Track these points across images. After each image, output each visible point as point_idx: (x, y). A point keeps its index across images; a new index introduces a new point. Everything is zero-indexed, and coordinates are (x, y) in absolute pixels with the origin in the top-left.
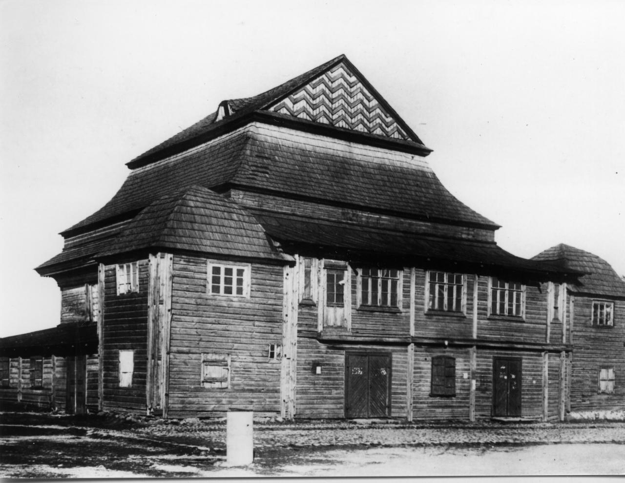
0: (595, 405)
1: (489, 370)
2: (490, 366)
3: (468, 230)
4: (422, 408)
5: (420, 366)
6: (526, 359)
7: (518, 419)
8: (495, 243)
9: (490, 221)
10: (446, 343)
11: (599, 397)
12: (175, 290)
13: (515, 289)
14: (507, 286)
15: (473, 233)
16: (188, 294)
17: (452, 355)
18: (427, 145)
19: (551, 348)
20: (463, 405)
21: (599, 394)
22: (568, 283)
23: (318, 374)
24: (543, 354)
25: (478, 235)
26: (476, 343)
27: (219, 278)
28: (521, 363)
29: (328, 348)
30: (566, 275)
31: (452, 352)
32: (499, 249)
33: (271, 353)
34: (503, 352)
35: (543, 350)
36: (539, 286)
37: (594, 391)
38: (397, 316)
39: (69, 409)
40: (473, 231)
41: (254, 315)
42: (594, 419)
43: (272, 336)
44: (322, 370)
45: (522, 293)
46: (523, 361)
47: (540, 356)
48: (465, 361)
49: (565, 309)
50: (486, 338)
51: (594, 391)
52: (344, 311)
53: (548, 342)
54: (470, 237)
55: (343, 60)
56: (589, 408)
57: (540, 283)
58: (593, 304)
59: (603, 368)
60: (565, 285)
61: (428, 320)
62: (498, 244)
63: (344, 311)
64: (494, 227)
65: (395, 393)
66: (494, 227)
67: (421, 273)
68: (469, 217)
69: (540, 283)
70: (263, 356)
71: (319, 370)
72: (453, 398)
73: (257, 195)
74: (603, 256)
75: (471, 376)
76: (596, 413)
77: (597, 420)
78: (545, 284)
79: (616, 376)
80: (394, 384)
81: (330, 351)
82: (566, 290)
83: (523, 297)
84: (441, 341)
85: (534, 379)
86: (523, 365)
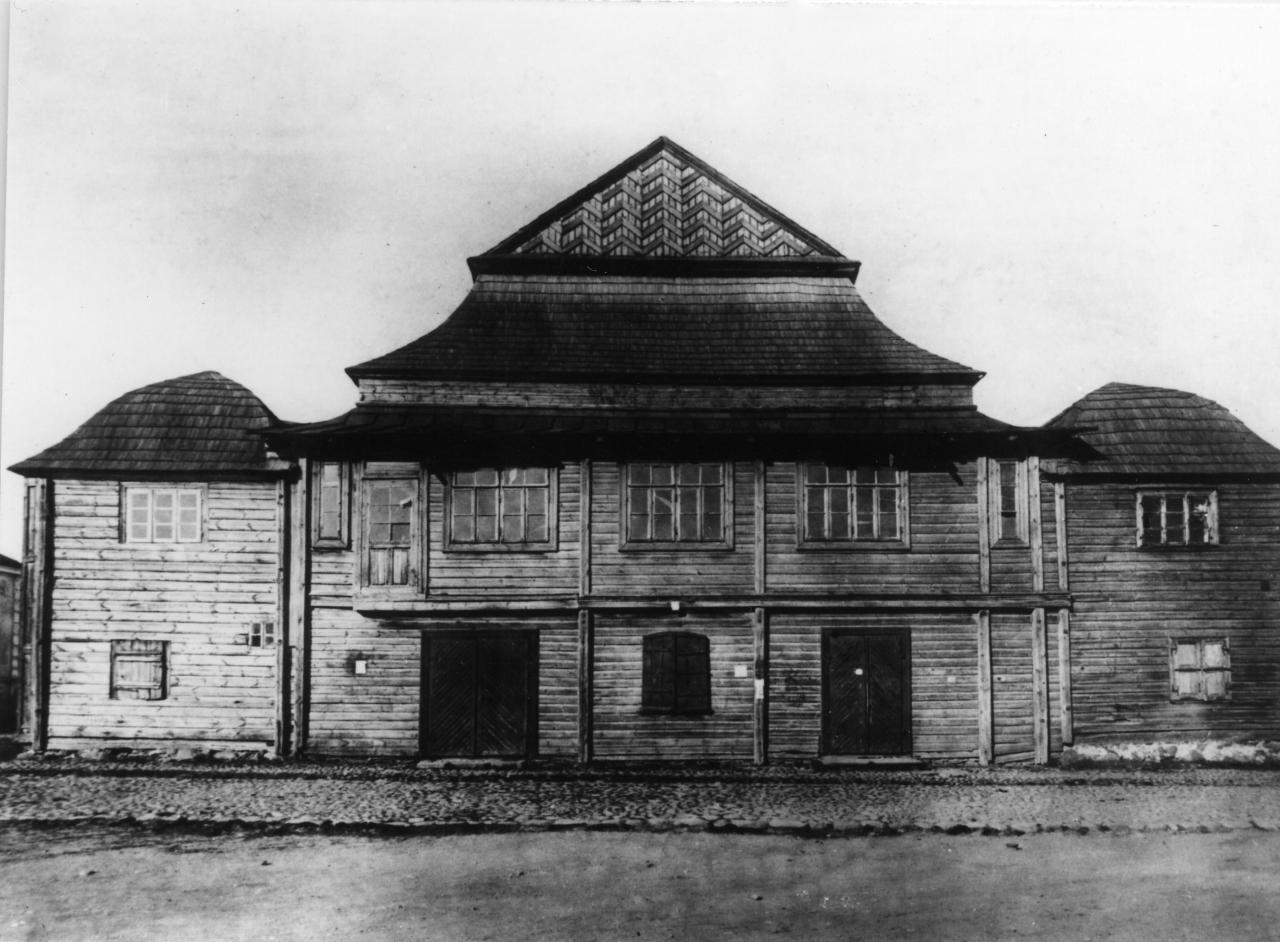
0: (1164, 727)
1: (811, 657)
2: (814, 649)
3: (901, 391)
4: (622, 738)
5: (617, 655)
6: (919, 630)
7: (906, 760)
8: (975, 408)
9: (964, 368)
10: (675, 606)
11: (1178, 709)
12: (321, 551)
13: (828, 483)
14: (851, 478)
15: (913, 395)
16: (87, 543)
17: (698, 630)
18: (850, 255)
19: (991, 603)
20: (131, 767)
21: (1173, 702)
22: (1042, 456)
23: (360, 675)
24: (976, 617)
25: (924, 396)
26: (759, 603)
27: (145, 512)
28: (910, 640)
29: (382, 625)
30: (1012, 438)
31: (701, 623)
32: (983, 417)
33: (254, 638)
34: (850, 618)
35: (975, 610)
36: (953, 471)
37: (1162, 697)
38: (547, 558)
39: (781, 698)
40: (914, 390)
41: (218, 573)
42: (1158, 759)
43: (255, 608)
44: (367, 667)
45: (897, 490)
46: (914, 635)
47: (970, 621)
48: (737, 642)
49: (1036, 514)
50: (795, 590)
51: (1162, 697)
52: (408, 556)
53: (986, 590)
54: (908, 403)
55: (661, 144)
56: (1144, 735)
57: (957, 465)
58: (1139, 500)
59: (1181, 643)
60: (1034, 461)
61: (629, 562)
62: (981, 410)
63: (408, 556)
64: (970, 378)
65: (546, 710)
66: (970, 378)
67: (743, 475)
68: (913, 366)
69: (957, 465)
70: (236, 644)
71: (360, 667)
72: (706, 717)
73: (409, 382)
74: (1205, 392)
75: (753, 672)
76: (1166, 746)
77: (1169, 764)
78: (970, 464)
79: (1232, 660)
80: (545, 692)
81: (386, 631)
82: (1036, 474)
83: (902, 500)
84: (659, 604)
85: (949, 673)
86: (914, 643)
